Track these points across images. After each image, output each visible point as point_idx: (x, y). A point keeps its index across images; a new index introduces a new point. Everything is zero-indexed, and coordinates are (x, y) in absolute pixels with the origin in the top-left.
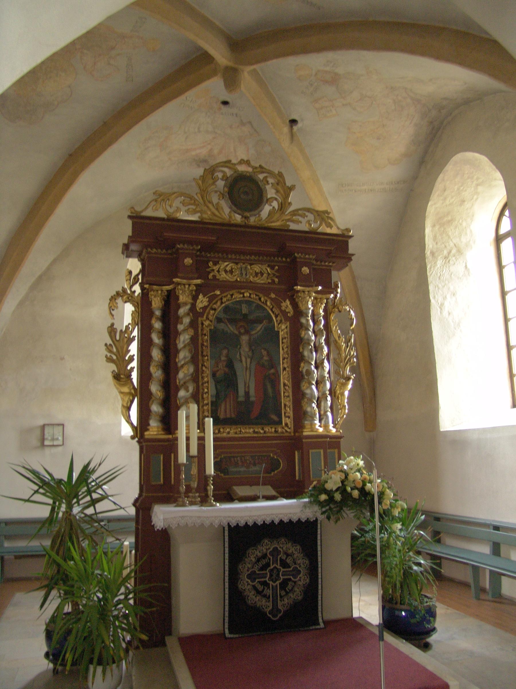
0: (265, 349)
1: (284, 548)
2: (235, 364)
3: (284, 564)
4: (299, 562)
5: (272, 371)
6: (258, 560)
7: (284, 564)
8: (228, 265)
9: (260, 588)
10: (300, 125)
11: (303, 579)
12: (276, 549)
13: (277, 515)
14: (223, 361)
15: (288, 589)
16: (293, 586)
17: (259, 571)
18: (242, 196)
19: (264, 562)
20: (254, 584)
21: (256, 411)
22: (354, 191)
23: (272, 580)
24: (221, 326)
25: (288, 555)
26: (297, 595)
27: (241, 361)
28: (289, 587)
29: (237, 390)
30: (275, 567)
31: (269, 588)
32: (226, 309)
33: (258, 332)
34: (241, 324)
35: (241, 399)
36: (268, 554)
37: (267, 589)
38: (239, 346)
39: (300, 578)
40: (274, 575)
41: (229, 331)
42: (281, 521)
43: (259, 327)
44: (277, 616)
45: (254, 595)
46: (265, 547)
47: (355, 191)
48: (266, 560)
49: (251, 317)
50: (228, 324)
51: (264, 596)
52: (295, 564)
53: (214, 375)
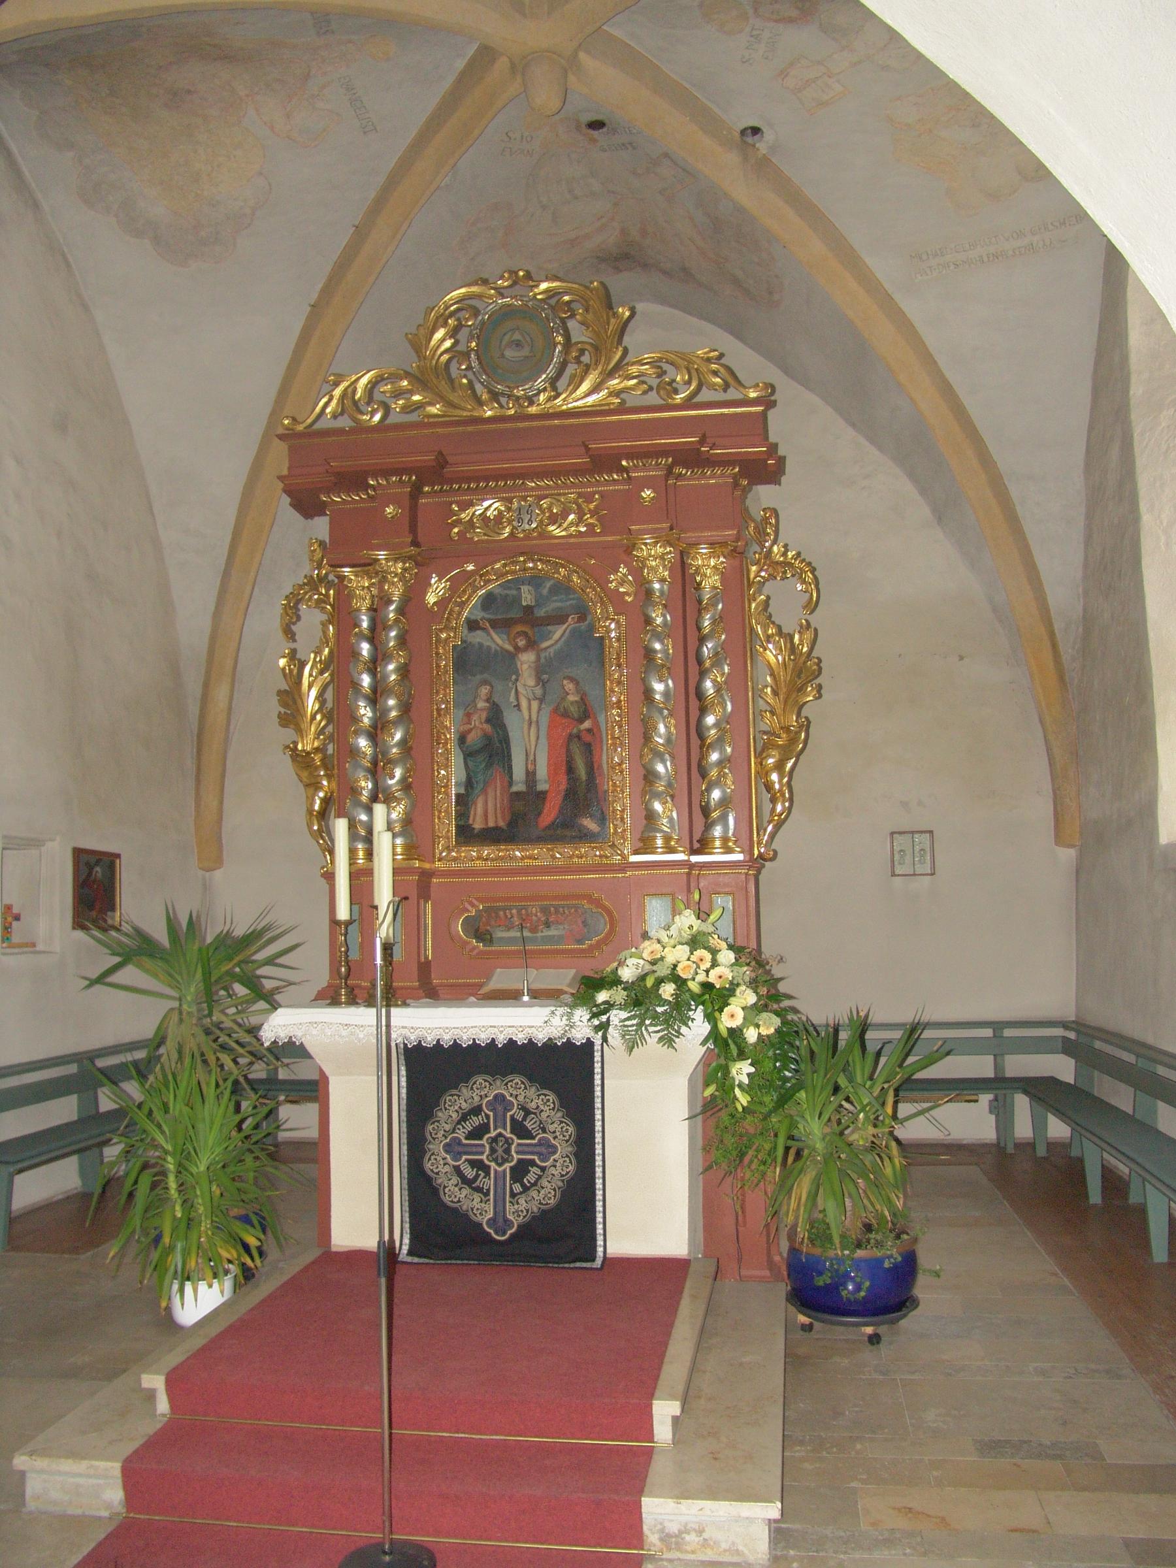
0: (571, 679)
1: (521, 1098)
2: (505, 714)
3: (520, 1130)
4: (552, 1128)
5: (587, 724)
6: (464, 1118)
7: (520, 1130)
8: (490, 506)
9: (469, 1173)
10: (769, 135)
11: (561, 1165)
12: (499, 1098)
13: (502, 1029)
14: (481, 710)
15: (529, 1182)
16: (540, 1177)
17: (466, 1138)
18: (509, 353)
19: (476, 1121)
20: (457, 1163)
21: (550, 813)
22: (952, 267)
23: (495, 1160)
24: (478, 637)
25: (527, 1112)
26: (546, 1194)
27: (518, 706)
28: (531, 1177)
29: (510, 767)
30: (500, 1135)
31: (488, 1174)
32: (489, 601)
33: (557, 641)
34: (519, 628)
35: (519, 787)
36: (484, 1106)
37: (485, 1177)
38: (514, 677)
39: (554, 1160)
40: (500, 1151)
41: (493, 646)
42: (511, 1042)
43: (558, 632)
44: (504, 1233)
45: (456, 1186)
46: (540, 1102)
47: (957, 266)
48: (480, 1119)
49: (541, 613)
50: (491, 631)
51: (479, 1190)
52: (544, 1130)
53: (462, 740)
